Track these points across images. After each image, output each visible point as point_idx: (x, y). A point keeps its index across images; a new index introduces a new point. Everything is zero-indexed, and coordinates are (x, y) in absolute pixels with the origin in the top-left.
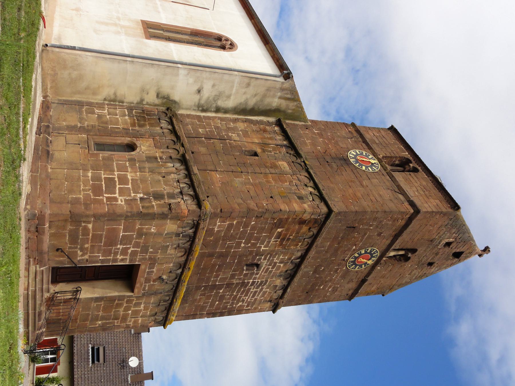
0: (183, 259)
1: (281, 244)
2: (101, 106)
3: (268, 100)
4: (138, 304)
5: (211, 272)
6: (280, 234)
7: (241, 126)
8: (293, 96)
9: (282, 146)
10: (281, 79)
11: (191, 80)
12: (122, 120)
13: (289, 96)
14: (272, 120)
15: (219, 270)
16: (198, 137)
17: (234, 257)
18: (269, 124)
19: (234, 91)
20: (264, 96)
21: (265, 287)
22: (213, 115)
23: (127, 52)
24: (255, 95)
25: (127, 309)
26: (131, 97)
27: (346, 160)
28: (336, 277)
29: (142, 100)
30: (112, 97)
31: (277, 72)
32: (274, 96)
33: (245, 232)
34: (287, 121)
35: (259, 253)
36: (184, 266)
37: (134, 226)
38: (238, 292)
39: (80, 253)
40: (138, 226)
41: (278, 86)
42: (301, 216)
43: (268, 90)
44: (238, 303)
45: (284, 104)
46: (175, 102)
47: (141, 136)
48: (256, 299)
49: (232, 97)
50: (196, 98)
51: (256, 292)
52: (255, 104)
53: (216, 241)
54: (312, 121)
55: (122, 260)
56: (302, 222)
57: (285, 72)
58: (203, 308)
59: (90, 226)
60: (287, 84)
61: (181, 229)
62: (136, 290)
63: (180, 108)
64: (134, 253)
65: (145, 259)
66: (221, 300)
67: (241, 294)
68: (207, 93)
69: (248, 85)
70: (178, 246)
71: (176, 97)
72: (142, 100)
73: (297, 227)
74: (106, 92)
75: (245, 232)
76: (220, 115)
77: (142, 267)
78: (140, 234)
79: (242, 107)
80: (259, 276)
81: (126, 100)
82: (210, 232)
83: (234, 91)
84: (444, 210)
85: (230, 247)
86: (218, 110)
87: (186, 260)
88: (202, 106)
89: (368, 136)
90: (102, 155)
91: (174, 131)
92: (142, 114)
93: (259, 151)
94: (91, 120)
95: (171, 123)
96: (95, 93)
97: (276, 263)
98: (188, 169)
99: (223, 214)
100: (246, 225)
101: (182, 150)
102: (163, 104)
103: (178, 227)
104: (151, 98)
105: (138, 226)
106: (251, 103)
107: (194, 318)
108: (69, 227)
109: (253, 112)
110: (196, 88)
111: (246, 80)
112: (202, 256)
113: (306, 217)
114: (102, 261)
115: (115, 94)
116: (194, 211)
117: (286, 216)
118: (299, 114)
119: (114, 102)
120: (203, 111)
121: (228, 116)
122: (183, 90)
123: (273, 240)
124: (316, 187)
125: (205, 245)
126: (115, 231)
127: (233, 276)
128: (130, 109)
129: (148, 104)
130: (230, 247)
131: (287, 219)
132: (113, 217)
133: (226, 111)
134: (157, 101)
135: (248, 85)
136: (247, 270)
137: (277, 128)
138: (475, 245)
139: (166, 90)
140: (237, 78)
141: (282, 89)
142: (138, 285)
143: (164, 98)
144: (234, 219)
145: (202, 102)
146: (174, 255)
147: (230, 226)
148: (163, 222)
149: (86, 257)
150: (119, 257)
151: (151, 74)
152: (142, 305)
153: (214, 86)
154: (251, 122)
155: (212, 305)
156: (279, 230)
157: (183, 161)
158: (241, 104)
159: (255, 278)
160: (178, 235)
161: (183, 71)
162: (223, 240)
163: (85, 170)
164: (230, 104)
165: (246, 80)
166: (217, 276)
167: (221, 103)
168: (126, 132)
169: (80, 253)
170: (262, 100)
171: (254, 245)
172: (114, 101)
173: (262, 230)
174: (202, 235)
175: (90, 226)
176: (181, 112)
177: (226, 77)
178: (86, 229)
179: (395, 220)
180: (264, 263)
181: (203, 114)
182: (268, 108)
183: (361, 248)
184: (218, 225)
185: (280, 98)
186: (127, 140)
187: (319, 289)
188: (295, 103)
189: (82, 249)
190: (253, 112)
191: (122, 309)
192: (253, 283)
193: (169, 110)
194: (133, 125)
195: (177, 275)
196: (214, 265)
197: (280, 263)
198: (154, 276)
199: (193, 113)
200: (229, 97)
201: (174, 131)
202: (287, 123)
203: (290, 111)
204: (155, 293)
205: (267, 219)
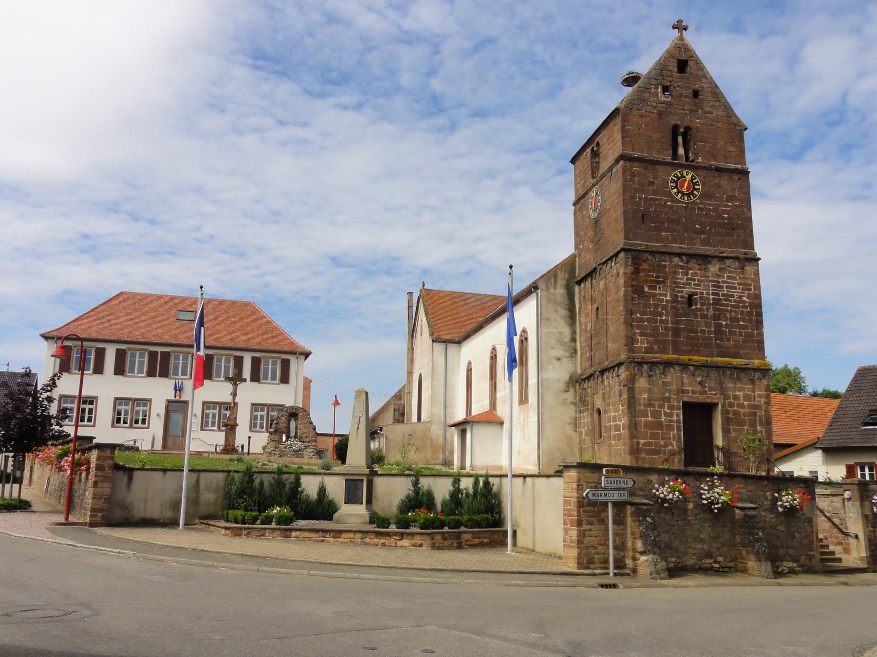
0: (677, 367)
1: (663, 282)
2: (581, 434)
3: (560, 299)
4: (736, 398)
5: (698, 338)
6: (650, 288)
7: (583, 318)
8: (551, 276)
9: (592, 284)
10: (539, 291)
11: (550, 367)
12: (586, 419)
13: (553, 281)
14: (577, 289)
15: (696, 332)
16: (591, 358)
17: (677, 322)
18: (580, 292)
19: (554, 330)
20: (556, 303)
21: (720, 280)
22: (578, 343)
23: (536, 418)
24: (556, 311)
25: (742, 406)
26: (571, 411)
27: (597, 221)
28: (710, 205)
29: (572, 403)
30: (573, 426)
31: (534, 296)
32: (554, 294)
33: (648, 320)
34: (577, 274)
35: (675, 299)
36: (684, 366)
37: (642, 411)
38: (727, 305)
39: (670, 447)
40: (642, 408)
41: (545, 293)
42: (629, 276)
43: (549, 301)
44: (745, 302)
45: (561, 283)
46: (571, 377)
47: (593, 404)
48: (738, 284)
49: (560, 330)
50: (565, 360)
51: (727, 287)
52: (564, 308)
53: (657, 342)
54: (576, 248)
55: (678, 416)
56: (636, 271)
57: (532, 289)
58: (749, 336)
59: (642, 441)
60: (542, 286)
61: (645, 375)
62: (715, 401)
63: (576, 372)
64: (671, 407)
65: (677, 399)
66: (738, 320)
67: (730, 301)
68: (559, 352)
69: (548, 320)
70: (663, 373)
71: (566, 377)
72: (572, 403)
73: (641, 274)
74: (569, 430)
75: (648, 320)
76: (578, 337)
77: (686, 399)
78: (650, 405)
79: (568, 319)
80: (707, 292)
81: (574, 415)
82: (648, 350)
83: (554, 330)
84: (620, 125)
85: (667, 329)
86: (574, 340)
87: (678, 364)
88: (572, 354)
89: (581, 192)
90: (604, 434)
91: (588, 378)
92: (582, 403)
93: (595, 306)
94: (587, 440)
95: (584, 380)
96: (571, 439)
97: (687, 279)
98: (608, 369)
99: (630, 341)
100: (643, 321)
101: (597, 373)
102: (574, 386)
103: (642, 376)
104: (570, 396)
105: (642, 408)
106: (564, 312)
107: (763, 341)
108: (644, 455)
109: (571, 309)
110: (556, 362)
111: (544, 322)
112: (676, 351)
113: (630, 269)
114: (679, 430)
115: (570, 424)
116: (626, 368)
117: (630, 289)
118: (569, 265)
119: (576, 424)
120: (575, 352)
121: (578, 330)
122: (560, 372)
123: (658, 292)
124: (610, 259)
125: (663, 351)
126: (647, 425)
127: (704, 316)
128: (581, 412)
129: (575, 398)
130: (667, 329)
131: (633, 286)
132: (633, 426)
133: (574, 333)
134: (572, 391)
135: (548, 320)
136: (696, 305)
137: (582, 285)
138: (667, 51)
139: (561, 386)
140: (544, 330)
141: (548, 289)
142: (709, 401)
143: (568, 386)
144: (635, 334)
145: (568, 354)
146: (672, 376)
147: (641, 334)
148: (637, 389)
149: (674, 443)
150: (675, 418)
151: (549, 399)
152: (737, 393)
153: (552, 348)
154: (580, 308)
155: (744, 327)
156: (646, 289)
157: (602, 372)
158: (565, 322)
159: (708, 294)
160: (650, 376)
161: (544, 375)
162: (658, 336)
163: (611, 445)
164: (566, 331)
165: (544, 322)
166: (703, 332)
167: (567, 338)
168: (592, 415)
169: (670, 447)
170: (560, 304)
171: (664, 307)
172: (576, 424)
173: (647, 305)
174: (650, 357)
175: (642, 441)
176: (579, 371)
177: (544, 340)
178: (645, 444)
179: (633, 175)
180: (687, 290)
181: (579, 352)
182: (566, 296)
183: (671, 195)
184: (642, 343)
185: (555, 288)
186: (596, 415)
187: (728, 219)
188: (559, 272)
189: (666, 446)
190: (571, 309)
191: (742, 411)
192: (713, 294)
193: (576, 381)
194: (588, 409)
195: (695, 369)
196: (688, 337)
197: (687, 274)
198: (699, 388)
199: (579, 360)
200: (560, 333)
201: (588, 378)
202: (579, 274)
203: (567, 275)
204: (721, 384)
205: (634, 304)
